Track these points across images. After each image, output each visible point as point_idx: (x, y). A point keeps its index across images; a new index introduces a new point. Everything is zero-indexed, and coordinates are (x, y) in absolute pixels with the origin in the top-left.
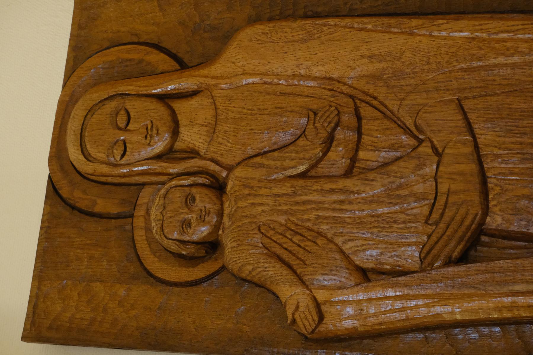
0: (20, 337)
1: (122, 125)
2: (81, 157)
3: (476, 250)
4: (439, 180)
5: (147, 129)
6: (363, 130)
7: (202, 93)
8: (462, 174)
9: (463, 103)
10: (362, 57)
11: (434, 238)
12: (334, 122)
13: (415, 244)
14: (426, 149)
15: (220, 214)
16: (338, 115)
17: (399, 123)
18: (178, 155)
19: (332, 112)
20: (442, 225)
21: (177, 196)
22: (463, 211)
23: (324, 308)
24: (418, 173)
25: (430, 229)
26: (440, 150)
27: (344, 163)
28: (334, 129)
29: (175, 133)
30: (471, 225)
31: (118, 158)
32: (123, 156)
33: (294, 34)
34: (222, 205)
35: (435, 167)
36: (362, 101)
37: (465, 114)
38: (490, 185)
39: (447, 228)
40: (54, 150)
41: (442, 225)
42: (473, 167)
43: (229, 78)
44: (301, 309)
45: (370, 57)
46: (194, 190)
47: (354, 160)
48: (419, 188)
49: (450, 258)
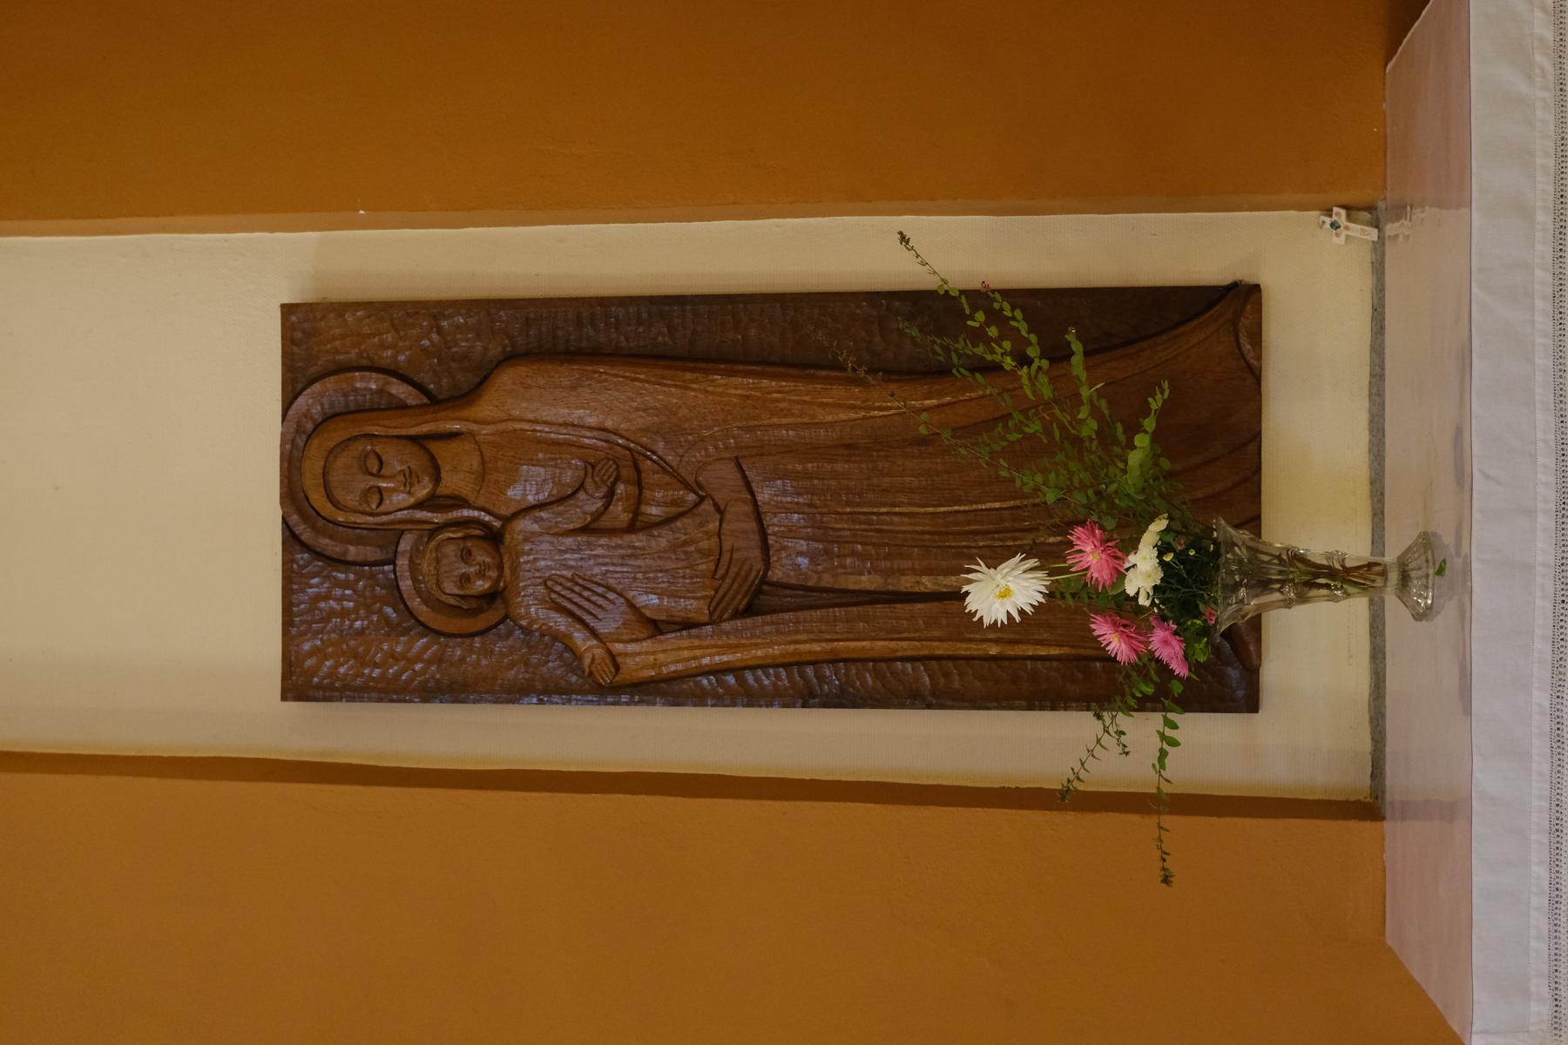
0: (280, 698)
1: (375, 471)
2: (329, 505)
3: (759, 599)
4: (723, 537)
5: (405, 475)
6: (643, 484)
7: (463, 436)
8: (744, 532)
9: (741, 461)
10: (637, 409)
11: (721, 592)
12: (614, 476)
13: (704, 597)
14: (707, 506)
15: (500, 567)
16: (617, 469)
17: (680, 478)
18: (441, 501)
19: (610, 466)
20: (728, 581)
21: (450, 549)
22: (746, 567)
23: (619, 659)
24: (702, 529)
25: (717, 583)
26: (722, 508)
27: (625, 518)
28: (614, 484)
29: (437, 479)
30: (755, 580)
31: (374, 506)
32: (379, 504)
33: (562, 379)
34: (501, 559)
35: (718, 524)
36: (640, 454)
37: (742, 472)
38: (770, 542)
39: (733, 582)
40: (285, 489)
41: (728, 581)
42: (754, 525)
43: (493, 423)
44: (597, 662)
45: (645, 410)
46: (469, 544)
47: (636, 513)
48: (705, 544)
49: (737, 610)
